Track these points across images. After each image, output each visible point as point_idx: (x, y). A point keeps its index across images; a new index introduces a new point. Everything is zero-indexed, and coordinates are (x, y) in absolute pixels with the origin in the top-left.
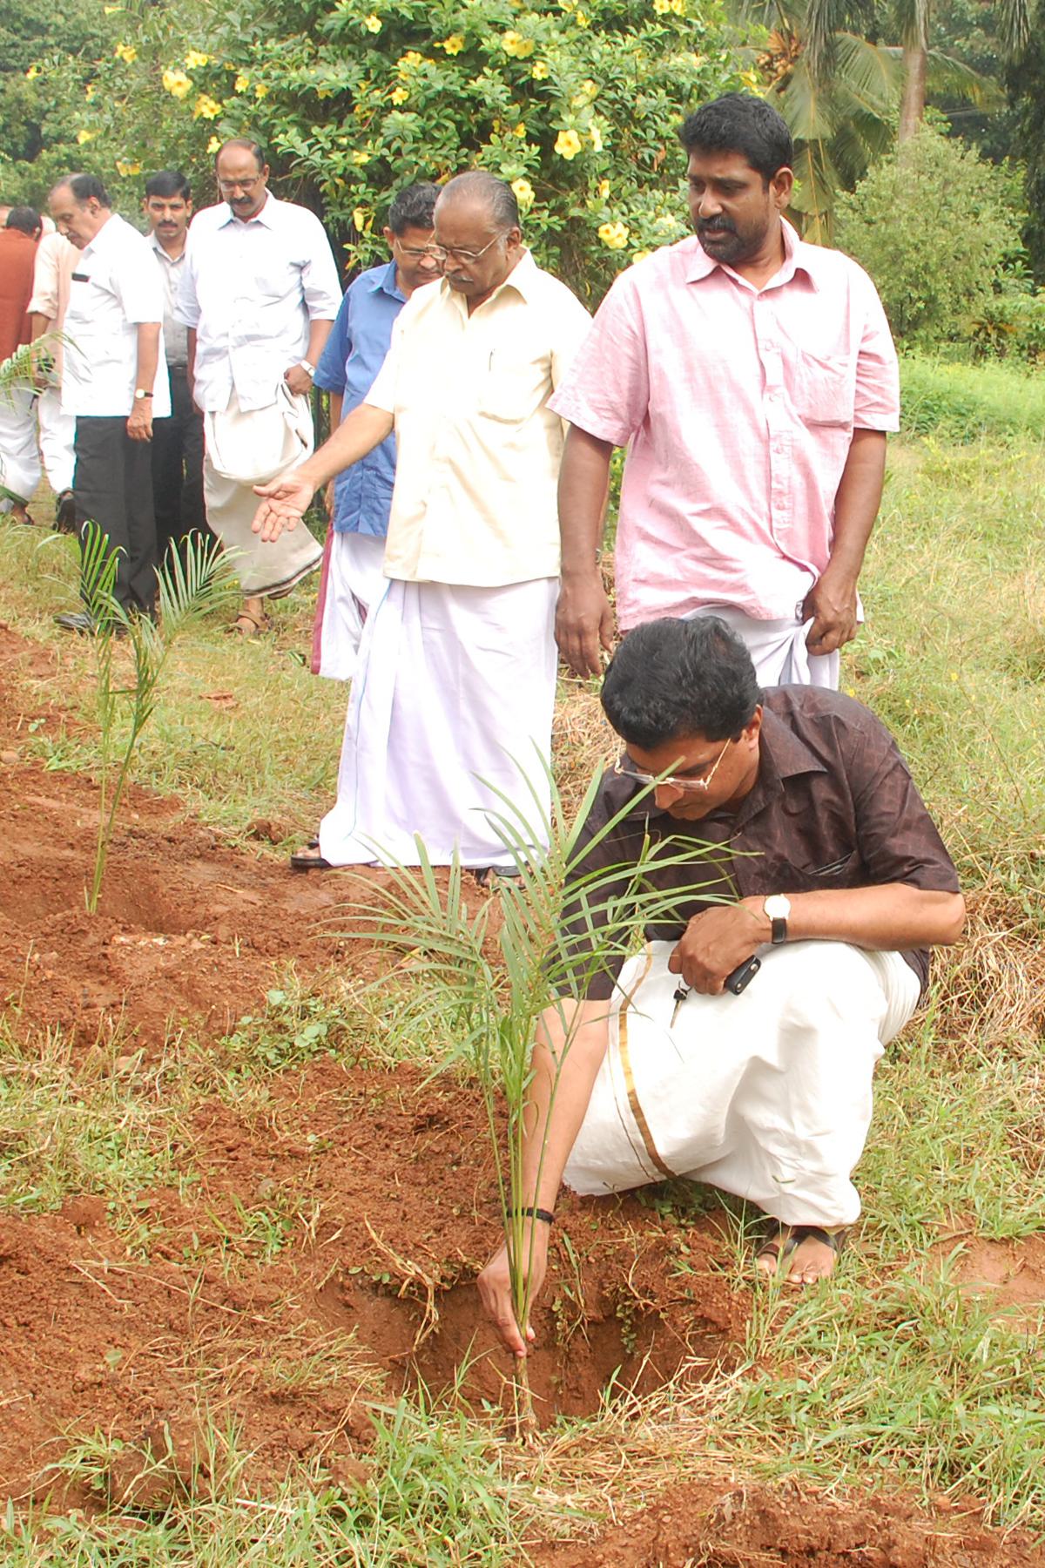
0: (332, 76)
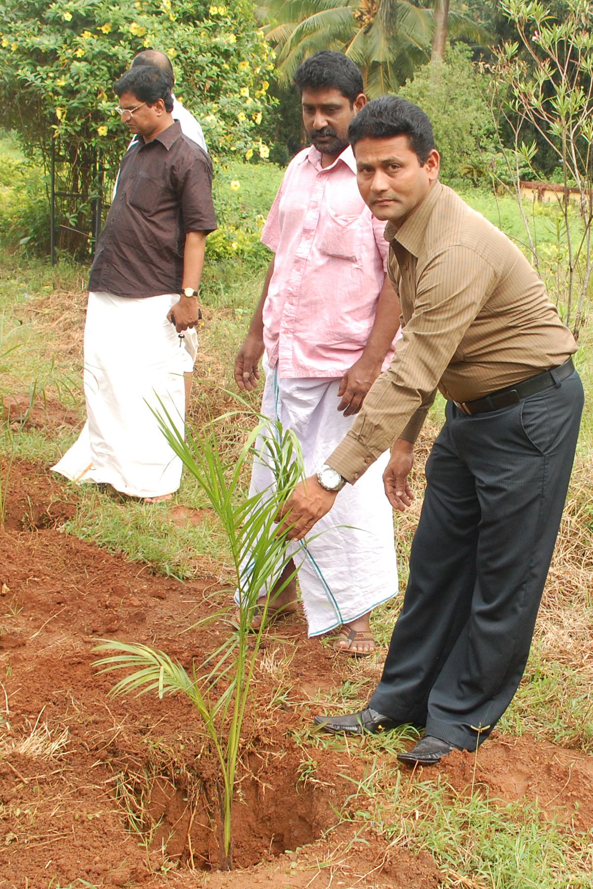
0: (47, 42)
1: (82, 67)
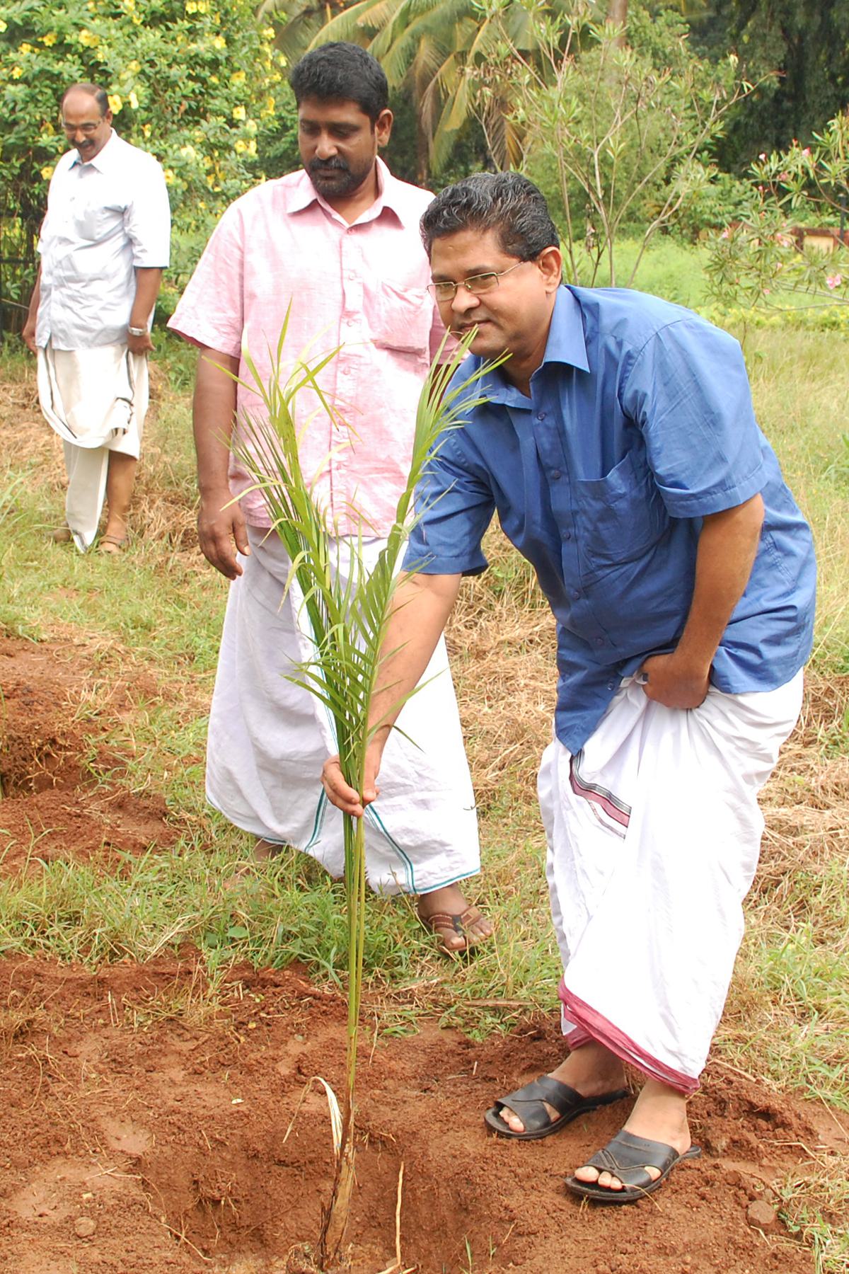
1: (18, 91)
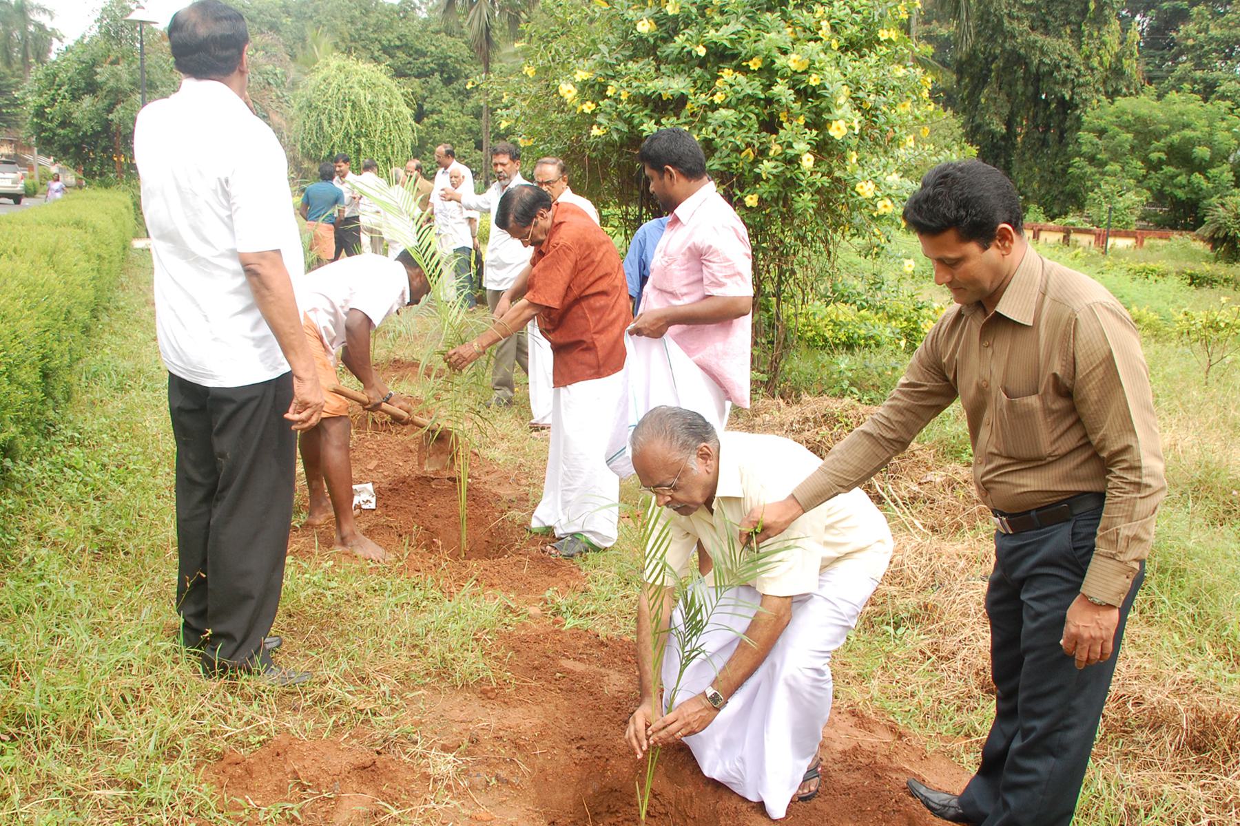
0: (676, 85)
